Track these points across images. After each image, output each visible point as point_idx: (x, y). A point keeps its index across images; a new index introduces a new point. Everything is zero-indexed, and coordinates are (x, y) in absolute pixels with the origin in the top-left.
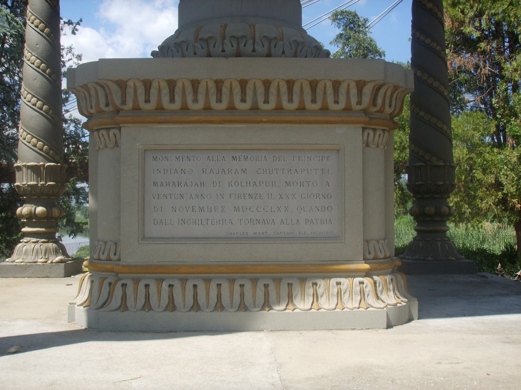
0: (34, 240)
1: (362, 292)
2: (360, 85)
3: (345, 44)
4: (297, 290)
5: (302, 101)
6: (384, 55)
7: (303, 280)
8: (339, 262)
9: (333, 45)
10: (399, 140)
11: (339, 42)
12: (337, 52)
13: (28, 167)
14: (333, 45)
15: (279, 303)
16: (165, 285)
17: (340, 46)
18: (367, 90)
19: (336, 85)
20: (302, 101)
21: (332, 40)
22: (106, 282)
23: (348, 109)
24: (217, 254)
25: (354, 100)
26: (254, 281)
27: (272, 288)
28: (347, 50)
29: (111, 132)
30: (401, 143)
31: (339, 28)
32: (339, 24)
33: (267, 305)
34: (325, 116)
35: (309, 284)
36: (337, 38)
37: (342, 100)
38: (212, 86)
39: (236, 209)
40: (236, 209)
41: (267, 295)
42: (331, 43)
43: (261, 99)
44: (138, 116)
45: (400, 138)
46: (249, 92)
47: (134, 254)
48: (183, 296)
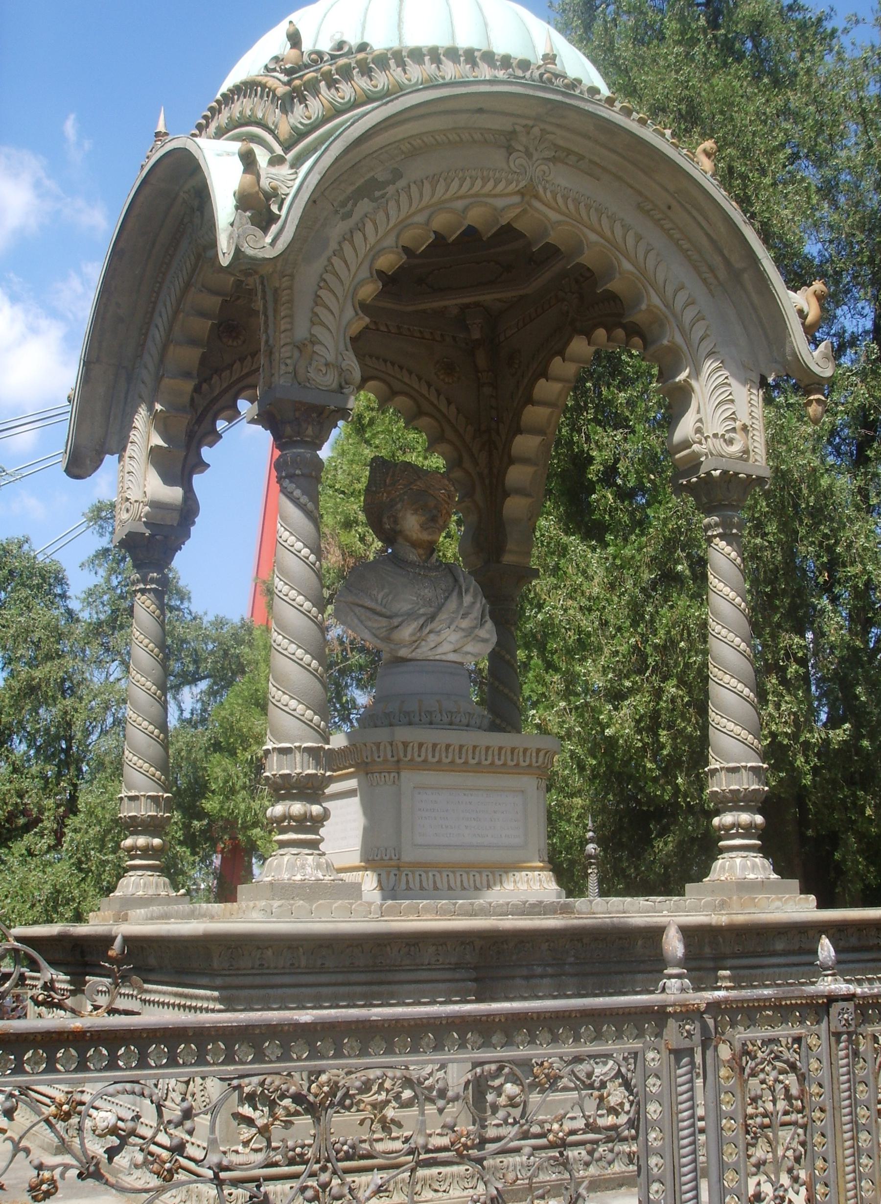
0: (150, 873)
1: (540, 881)
2: (538, 751)
3: (113, 571)
4: (504, 878)
5: (506, 760)
6: (189, 598)
7: (506, 872)
8: (525, 862)
9: (86, 571)
10: (223, 774)
11: (100, 565)
12: (95, 586)
13: (149, 797)
14: (86, 571)
15: (495, 884)
16: (430, 874)
17: (102, 572)
18: (542, 754)
19: (525, 751)
20: (506, 760)
21: (84, 558)
22: (392, 875)
23: (530, 766)
24: (457, 856)
25: (534, 760)
26: (480, 873)
27: (491, 877)
28: (115, 583)
29: (392, 775)
30: (227, 781)
31: (102, 535)
32: (101, 527)
33: (489, 887)
34: (517, 770)
35: (511, 874)
36: (95, 556)
37: (528, 760)
38: (457, 748)
39: (466, 827)
40: (466, 827)
41: (488, 881)
42: (82, 566)
43: (483, 758)
44: (414, 766)
45: (224, 770)
46: (477, 753)
47: (408, 856)
48: (442, 883)
